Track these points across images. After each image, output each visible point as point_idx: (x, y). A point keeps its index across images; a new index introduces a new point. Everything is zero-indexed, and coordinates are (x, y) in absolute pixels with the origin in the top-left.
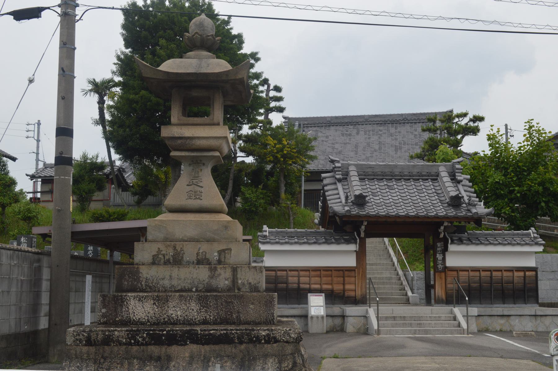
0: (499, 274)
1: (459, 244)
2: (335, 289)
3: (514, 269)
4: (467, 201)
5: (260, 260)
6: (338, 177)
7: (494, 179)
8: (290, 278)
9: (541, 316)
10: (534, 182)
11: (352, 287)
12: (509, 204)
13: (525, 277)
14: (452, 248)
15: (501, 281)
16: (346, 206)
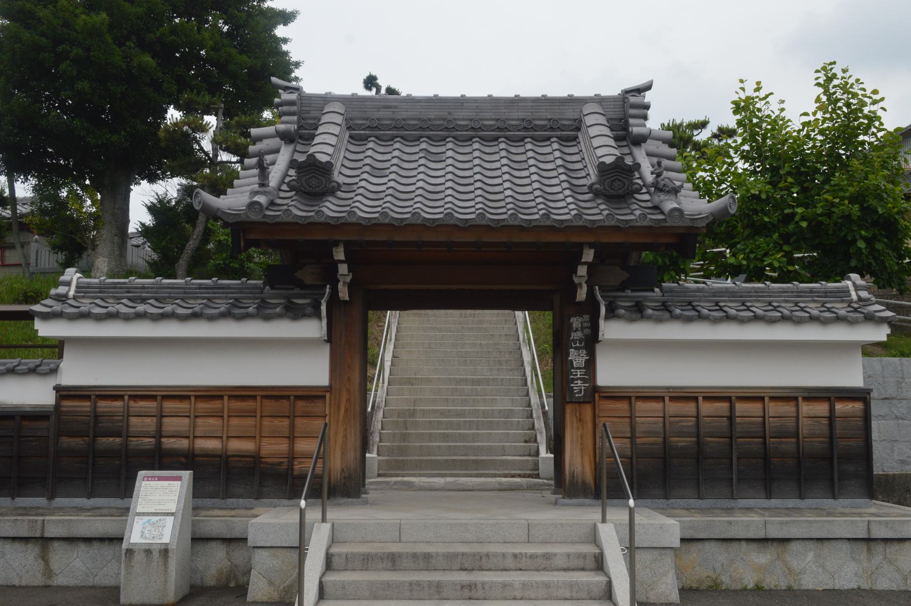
0: (755, 408)
1: (632, 320)
2: (263, 453)
3: (800, 395)
4: (650, 178)
7: (748, 191)
8: (134, 420)
10: (841, 194)
12: (781, 246)
13: (831, 417)
14: (610, 330)
15: (762, 431)
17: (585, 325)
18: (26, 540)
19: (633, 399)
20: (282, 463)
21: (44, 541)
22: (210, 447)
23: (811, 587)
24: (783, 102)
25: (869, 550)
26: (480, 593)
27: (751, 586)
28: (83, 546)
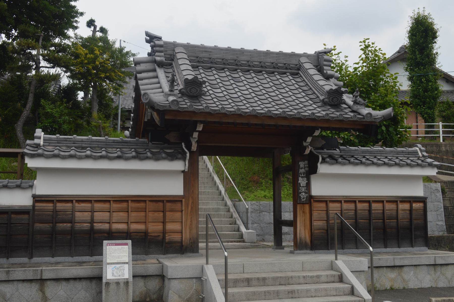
2: (150, 231)
3: (398, 200)
5: (27, 185)
6: (158, 59)
8: (77, 214)
9: (442, 265)
10: (375, 104)
11: (175, 226)
13: (411, 210)
16: (170, 95)
17: (306, 166)
18: (31, 281)
19: (328, 202)
20: (159, 235)
21: (42, 281)
22: (121, 228)
23: (412, 287)
24: (347, 57)
25: (435, 269)
26: (297, 295)
27: (388, 288)
28: (64, 283)
